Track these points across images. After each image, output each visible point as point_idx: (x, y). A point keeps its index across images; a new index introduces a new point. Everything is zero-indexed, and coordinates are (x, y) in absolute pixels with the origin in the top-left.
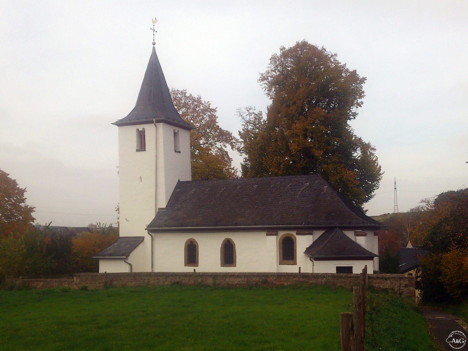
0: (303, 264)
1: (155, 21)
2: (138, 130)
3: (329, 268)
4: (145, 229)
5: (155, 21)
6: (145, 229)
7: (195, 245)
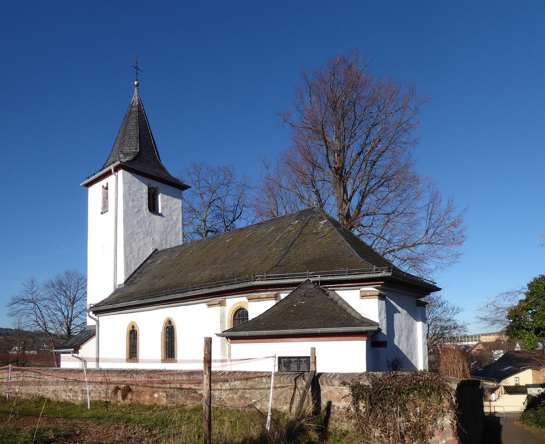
2: (103, 186)
3: (261, 356)
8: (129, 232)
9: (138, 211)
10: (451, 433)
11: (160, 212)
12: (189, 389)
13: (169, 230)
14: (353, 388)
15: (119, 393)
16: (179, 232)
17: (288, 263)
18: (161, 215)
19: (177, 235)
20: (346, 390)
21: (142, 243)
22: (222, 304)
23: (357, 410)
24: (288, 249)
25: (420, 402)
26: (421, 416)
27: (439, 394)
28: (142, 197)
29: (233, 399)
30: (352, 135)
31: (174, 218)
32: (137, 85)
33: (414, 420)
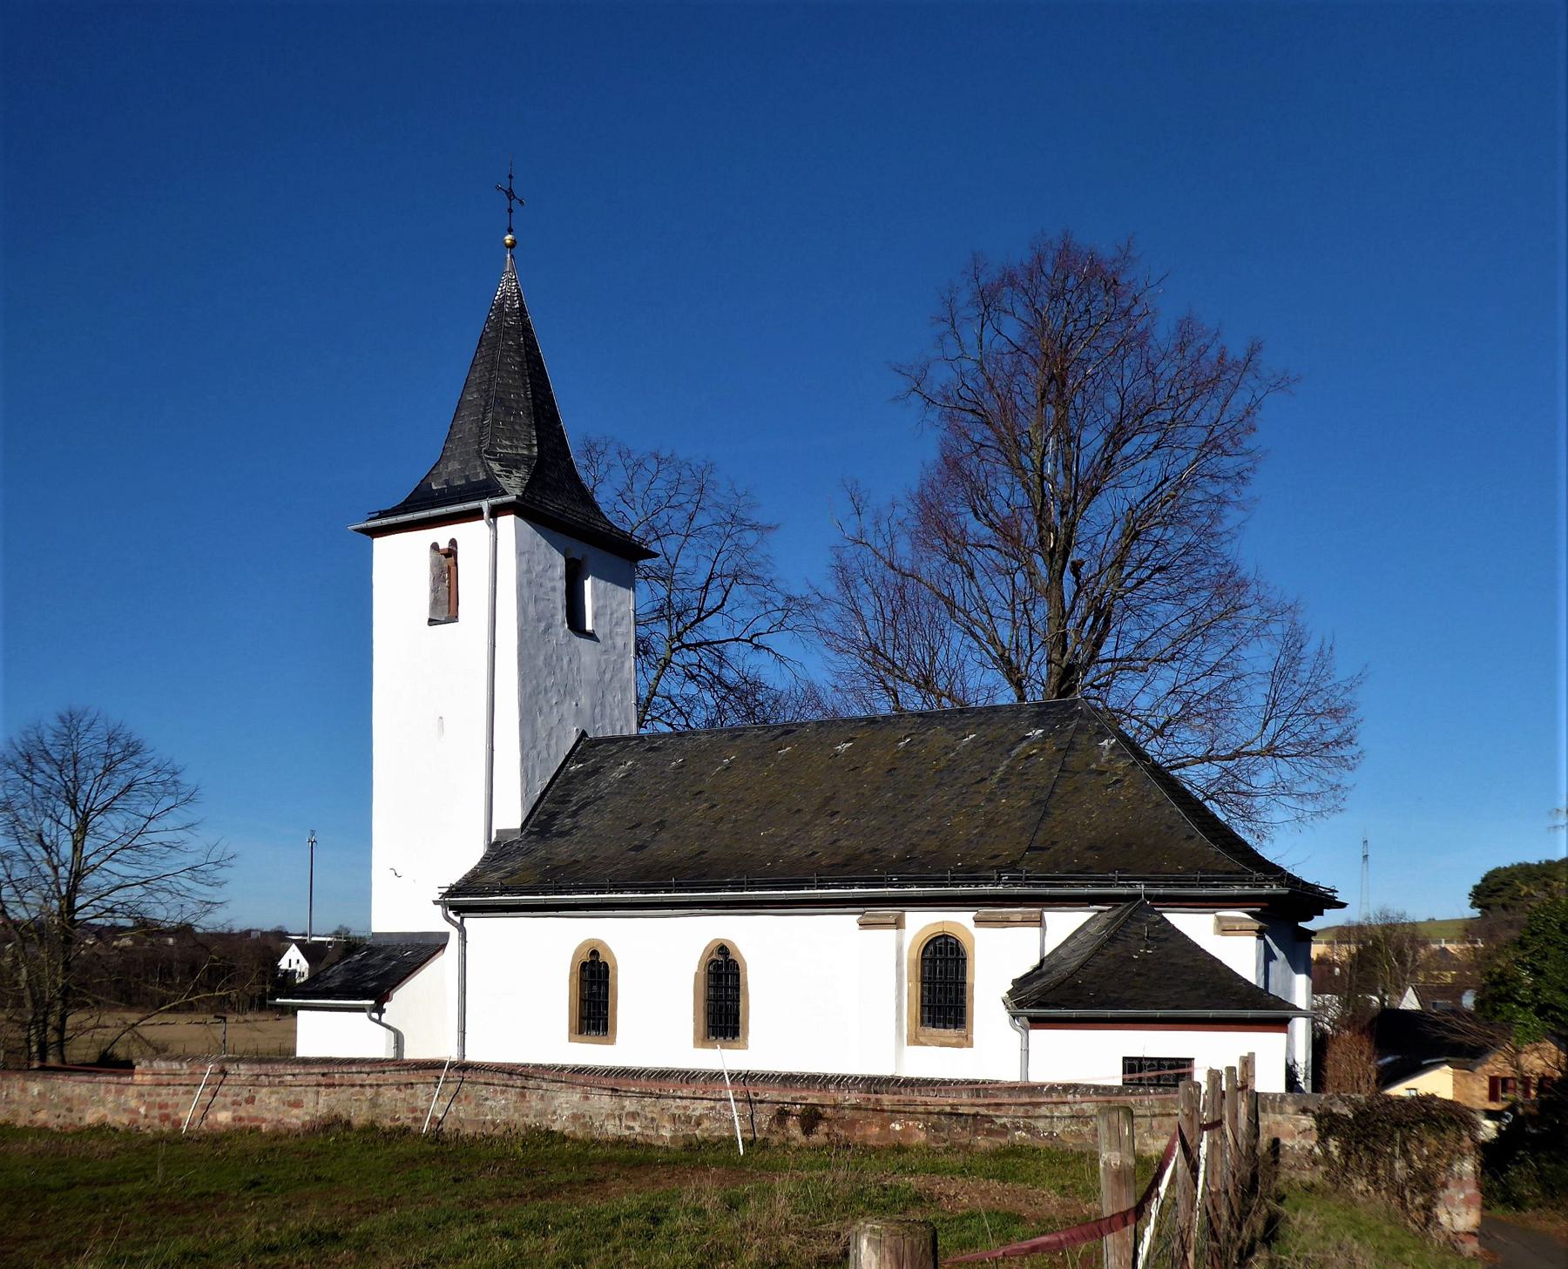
0: (995, 1049)
1: (313, 833)
2: (435, 547)
3: (1090, 1056)
4: (435, 903)
5: (313, 833)
6: (435, 903)
7: (606, 965)
8: (529, 690)
9: (548, 627)
10: (1473, 1184)
11: (589, 627)
12: (975, 1115)
13: (608, 676)
14: (1318, 1118)
15: (792, 1122)
16: (629, 681)
17: (1054, 843)
18: (591, 636)
19: (624, 690)
22: (898, 924)
23: (1327, 1153)
24: (1043, 806)
26: (1428, 1159)
27: (1459, 1129)
28: (554, 589)
29: (1080, 1134)
30: (1079, 439)
31: (619, 642)
32: (512, 246)
33: (1418, 1165)
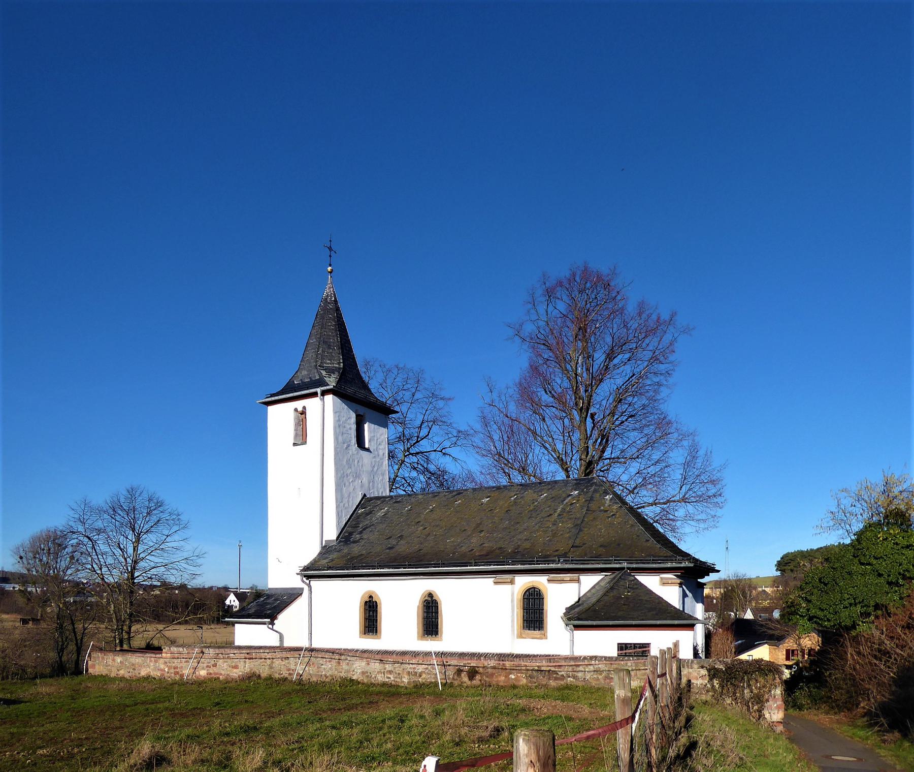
2: (296, 410)
11: (367, 446)
14: (709, 671)
18: (368, 450)
19: (383, 475)
20: (704, 672)
21: (351, 489)
22: (512, 582)
23: (713, 686)
24: (579, 527)
25: (761, 680)
26: (760, 688)
28: (350, 429)
30: (593, 353)
32: (330, 272)
33: (755, 691)
